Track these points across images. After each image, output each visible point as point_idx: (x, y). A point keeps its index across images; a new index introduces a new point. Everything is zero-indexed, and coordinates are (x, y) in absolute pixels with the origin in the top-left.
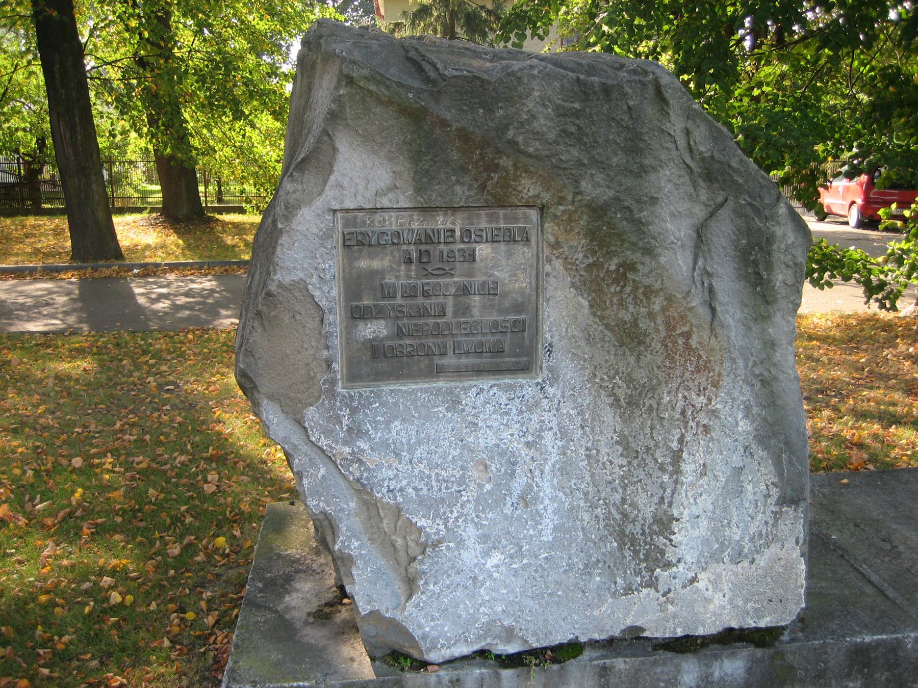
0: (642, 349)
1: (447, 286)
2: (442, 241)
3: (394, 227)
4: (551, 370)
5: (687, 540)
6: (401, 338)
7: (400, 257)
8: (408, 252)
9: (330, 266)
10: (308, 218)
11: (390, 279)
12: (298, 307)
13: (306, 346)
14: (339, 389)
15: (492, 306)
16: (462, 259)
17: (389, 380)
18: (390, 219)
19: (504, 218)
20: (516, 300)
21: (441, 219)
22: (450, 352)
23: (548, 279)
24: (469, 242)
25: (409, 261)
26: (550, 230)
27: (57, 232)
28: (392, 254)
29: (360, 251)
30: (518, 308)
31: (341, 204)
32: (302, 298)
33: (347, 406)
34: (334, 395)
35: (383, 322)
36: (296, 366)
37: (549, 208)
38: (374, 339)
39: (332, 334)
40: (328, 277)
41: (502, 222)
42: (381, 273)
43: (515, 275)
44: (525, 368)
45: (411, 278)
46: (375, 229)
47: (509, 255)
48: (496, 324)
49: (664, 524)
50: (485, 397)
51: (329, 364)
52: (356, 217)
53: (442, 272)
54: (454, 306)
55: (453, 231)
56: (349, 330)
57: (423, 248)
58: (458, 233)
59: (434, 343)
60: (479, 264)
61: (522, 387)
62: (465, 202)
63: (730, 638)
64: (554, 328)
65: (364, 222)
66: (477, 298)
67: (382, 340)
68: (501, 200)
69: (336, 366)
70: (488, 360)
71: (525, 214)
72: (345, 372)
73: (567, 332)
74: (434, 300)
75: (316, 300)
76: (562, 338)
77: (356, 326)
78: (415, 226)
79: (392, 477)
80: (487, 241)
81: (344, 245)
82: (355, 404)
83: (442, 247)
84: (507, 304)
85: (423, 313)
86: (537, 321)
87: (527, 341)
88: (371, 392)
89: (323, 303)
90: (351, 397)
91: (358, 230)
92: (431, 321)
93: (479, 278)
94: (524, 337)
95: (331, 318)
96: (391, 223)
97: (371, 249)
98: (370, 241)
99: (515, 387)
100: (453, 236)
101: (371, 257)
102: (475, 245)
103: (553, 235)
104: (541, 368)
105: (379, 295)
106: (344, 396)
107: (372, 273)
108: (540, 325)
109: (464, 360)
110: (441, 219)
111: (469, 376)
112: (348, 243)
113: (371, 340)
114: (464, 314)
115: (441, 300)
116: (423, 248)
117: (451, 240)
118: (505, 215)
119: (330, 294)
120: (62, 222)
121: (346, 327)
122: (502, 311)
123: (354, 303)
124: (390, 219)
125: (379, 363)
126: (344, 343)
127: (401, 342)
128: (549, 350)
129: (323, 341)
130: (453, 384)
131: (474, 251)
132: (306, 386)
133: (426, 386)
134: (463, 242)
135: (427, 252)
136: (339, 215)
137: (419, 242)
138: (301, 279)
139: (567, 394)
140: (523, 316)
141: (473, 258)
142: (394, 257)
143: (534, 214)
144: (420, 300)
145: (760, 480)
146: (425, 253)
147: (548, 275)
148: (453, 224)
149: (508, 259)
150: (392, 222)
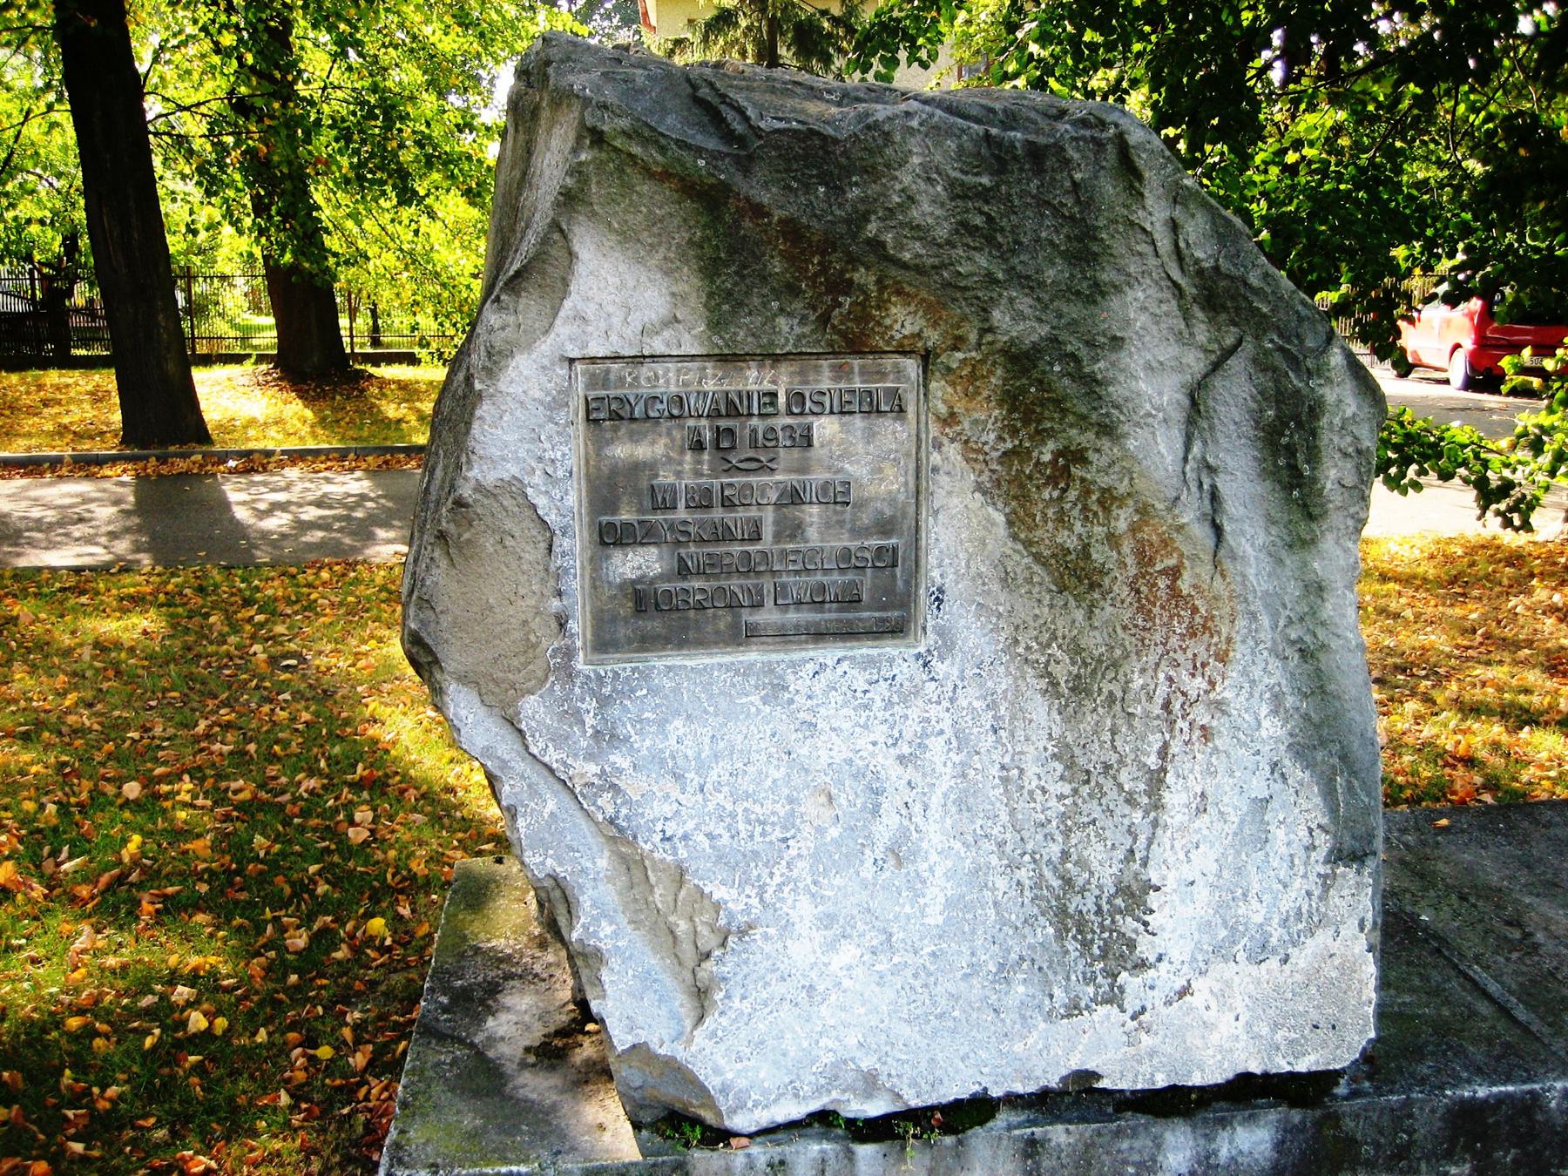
0: (1093, 578)
1: (763, 488)
2: (756, 411)
3: (673, 389)
4: (941, 632)
5: (1173, 927)
6: (684, 578)
7: (683, 439)
8: (697, 431)
9: (564, 455)
11: (666, 478)
12: (509, 525)
14: (580, 664)
15: (841, 523)
16: (788, 443)
17: (664, 649)
20: (882, 513)
21: (752, 373)
22: (769, 602)
23: (937, 477)
24: (802, 414)
25: (698, 447)
27: (97, 397)
28: (669, 434)
29: (615, 430)
30: (885, 526)
31: (582, 348)
33: (593, 694)
35: (654, 550)
36: (505, 626)
37: (938, 356)
38: (639, 580)
39: (566, 571)
40: (560, 474)
41: (857, 379)
42: (651, 467)
43: (880, 470)
44: (897, 630)
45: (702, 475)
47: (870, 436)
48: (846, 554)
49: (1134, 896)
50: (830, 676)
51: (562, 622)
52: (608, 372)
53: (754, 465)
54: (776, 523)
55: (774, 395)
56: (596, 564)
57: (723, 423)
58: (782, 399)
60: (818, 451)
61: (891, 661)
63: (1247, 1092)
64: (947, 561)
65: (622, 380)
66: (815, 509)
67: (652, 581)
68: (855, 341)
69: (574, 626)
70: (834, 616)
71: (896, 365)
72: (589, 636)
73: (968, 567)
74: (741, 513)
75: (540, 512)
76: (959, 578)
77: (608, 557)
78: (710, 386)
79: (665, 811)
80: (832, 412)
81: (588, 420)
82: (606, 691)
83: (755, 421)
84: (866, 519)
85: (723, 534)
87: (900, 583)
89: (552, 518)
90: (600, 678)
91: (612, 393)
92: (736, 549)
93: (818, 476)
94: (894, 576)
95: (566, 543)
96: (668, 382)
97: (634, 426)
98: (632, 412)
99: (880, 662)
100: (773, 404)
101: (634, 438)
102: (810, 419)
103: (944, 402)
104: (924, 629)
105: (647, 503)
106: (588, 677)
107: (636, 467)
108: (922, 554)
109: (793, 616)
110: (752, 373)
111: (800, 643)
112: (594, 416)
113: (633, 582)
114: (793, 537)
115: (753, 512)
116: (723, 423)
117: (770, 410)
118: (862, 367)
119: (564, 503)
120: (107, 380)
121: (591, 560)
122: (856, 532)
123: (605, 519)
125: (648, 620)
126: (587, 586)
127: (685, 585)
128: (937, 599)
129: (552, 582)
130: (774, 657)
131: (809, 428)
132: (522, 659)
133: (727, 659)
134: (790, 413)
135: (730, 431)
136: (579, 367)
137: (715, 414)
138: (514, 477)
139: (969, 673)
140: (893, 541)
141: (807, 441)
142: (673, 440)
143: (911, 366)
144: (718, 513)
145: (1300, 818)
146: (726, 433)
147: (935, 470)
148: (774, 382)
149: (869, 443)
150: (668, 380)
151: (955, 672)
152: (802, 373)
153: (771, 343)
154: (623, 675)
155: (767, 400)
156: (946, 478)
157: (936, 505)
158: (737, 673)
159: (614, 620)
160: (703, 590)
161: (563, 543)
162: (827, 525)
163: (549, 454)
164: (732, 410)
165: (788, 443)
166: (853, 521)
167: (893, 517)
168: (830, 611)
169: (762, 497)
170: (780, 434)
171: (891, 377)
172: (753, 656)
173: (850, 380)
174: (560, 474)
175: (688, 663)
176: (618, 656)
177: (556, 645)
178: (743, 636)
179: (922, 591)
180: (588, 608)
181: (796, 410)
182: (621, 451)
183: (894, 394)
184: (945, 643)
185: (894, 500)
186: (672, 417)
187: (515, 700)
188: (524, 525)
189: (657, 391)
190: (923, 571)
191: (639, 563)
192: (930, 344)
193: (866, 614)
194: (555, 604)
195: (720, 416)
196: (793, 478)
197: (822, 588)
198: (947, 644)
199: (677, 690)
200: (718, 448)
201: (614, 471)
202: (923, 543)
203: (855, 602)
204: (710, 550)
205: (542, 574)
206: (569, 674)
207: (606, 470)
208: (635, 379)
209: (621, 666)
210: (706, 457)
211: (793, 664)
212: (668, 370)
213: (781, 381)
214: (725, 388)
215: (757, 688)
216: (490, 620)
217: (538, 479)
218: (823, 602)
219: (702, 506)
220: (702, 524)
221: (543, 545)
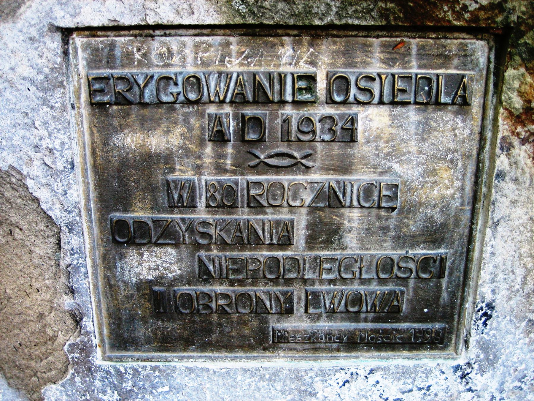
1: (296, 189)
2: (289, 98)
3: (191, 69)
4: (485, 347)
6: (206, 282)
7: (202, 129)
8: (218, 120)
9: (63, 144)
10: (11, 45)
11: (183, 173)
12: (14, 217)
13: (36, 285)
14: (98, 359)
15: (385, 229)
16: (327, 137)
17: (185, 350)
18: (181, 51)
19: (420, 57)
20: (431, 220)
21: (286, 51)
22: (299, 309)
23: (502, 184)
24: (344, 103)
25: (220, 138)
26: (516, 84)
28: (186, 121)
29: (126, 115)
30: (434, 235)
31: (74, 16)
32: (19, 201)
33: (114, 387)
34: (90, 370)
35: (171, 251)
36: (23, 317)
37: (522, 34)
38: (157, 281)
39: (76, 269)
40: (60, 165)
41: (414, 63)
42: (167, 159)
43: (434, 172)
44: (437, 342)
45: (225, 171)
46: (151, 71)
47: (425, 131)
48: (387, 265)
51: (77, 318)
52: (112, 46)
53: (286, 162)
54: (310, 226)
55: (311, 79)
56: (109, 263)
57: (249, 111)
58: (321, 85)
59: (268, 293)
60: (362, 149)
61: (428, 373)
62: (339, 16)
64: (501, 276)
65: (128, 56)
66: (356, 214)
67: (171, 284)
69: (90, 324)
70: (370, 326)
71: (462, 47)
72: (106, 332)
73: (524, 283)
74: (270, 216)
75: (43, 206)
76: (512, 293)
77: (122, 256)
78: (234, 66)
80: (381, 102)
81: (92, 104)
82: (128, 385)
83: (288, 110)
84: (413, 226)
85: (249, 238)
86: (468, 260)
87: (445, 295)
88: (154, 369)
89: (56, 213)
90: (119, 374)
91: (117, 72)
92: (264, 254)
93: (361, 177)
94: (439, 288)
95: (75, 241)
96: (183, 59)
97: (145, 112)
98: (142, 95)
99: (416, 372)
100: (310, 89)
101: (146, 125)
102: (355, 109)
103: (521, 94)
104: (466, 342)
105: (163, 199)
106: (108, 372)
107: (148, 160)
108: (474, 266)
109: (324, 325)
110: (286, 51)
111: (331, 350)
112: (98, 98)
113: (150, 282)
114: (328, 243)
115: (284, 215)
116: (249, 111)
117: (307, 97)
118: (421, 48)
121: (104, 258)
122: (400, 240)
123: (117, 215)
124: (181, 51)
126: (100, 285)
127: (206, 289)
128: (485, 314)
129: (63, 279)
130: (303, 365)
131: (353, 120)
132: (43, 350)
133: (252, 364)
134: (331, 101)
135: (257, 122)
136: (78, 41)
137: (239, 101)
138: (11, 167)
139: (509, 385)
140: (442, 251)
141: (350, 135)
142: (190, 130)
143: (480, 50)
144: (243, 215)
146: (252, 124)
147: (501, 175)
148: (313, 63)
149: (423, 140)
150: (185, 57)
151: (494, 385)
152: (347, 52)
153: (308, 11)
154: (143, 372)
155: (302, 84)
156: (512, 186)
157: (497, 215)
158: (262, 378)
159: (132, 319)
160: (226, 296)
161: (71, 241)
162: (369, 231)
163: (46, 143)
164: (261, 97)
165: (327, 137)
166: (399, 228)
167: (443, 226)
168: (366, 320)
169: (295, 198)
170: (318, 126)
171: (456, 61)
172: (280, 362)
173: (405, 64)
174: (60, 165)
175: (210, 365)
176: (137, 354)
177: (72, 341)
178: (265, 341)
179: (468, 305)
180: (103, 307)
181: (337, 99)
182: (130, 140)
183: (458, 83)
184: (487, 358)
185: (447, 206)
186: (188, 102)
187: (39, 386)
188: (31, 217)
189: (171, 71)
190: (472, 284)
191: (146, 265)
192: (514, 18)
193: (404, 325)
194: (68, 301)
195: (245, 102)
196: (330, 178)
197: (357, 300)
198: (490, 356)
199: (200, 389)
200: (243, 141)
201: (125, 163)
202: (476, 254)
203: (394, 314)
204: (235, 254)
205: (54, 269)
206: (90, 370)
207: (115, 162)
208: (144, 55)
209: (132, 363)
210: (229, 150)
211: (322, 373)
212: (184, 45)
213: (323, 62)
214: (253, 68)
215: (283, 392)
216: (8, 309)
217: (36, 170)
218: (359, 312)
219: (224, 206)
220: (226, 226)
221: (52, 240)
